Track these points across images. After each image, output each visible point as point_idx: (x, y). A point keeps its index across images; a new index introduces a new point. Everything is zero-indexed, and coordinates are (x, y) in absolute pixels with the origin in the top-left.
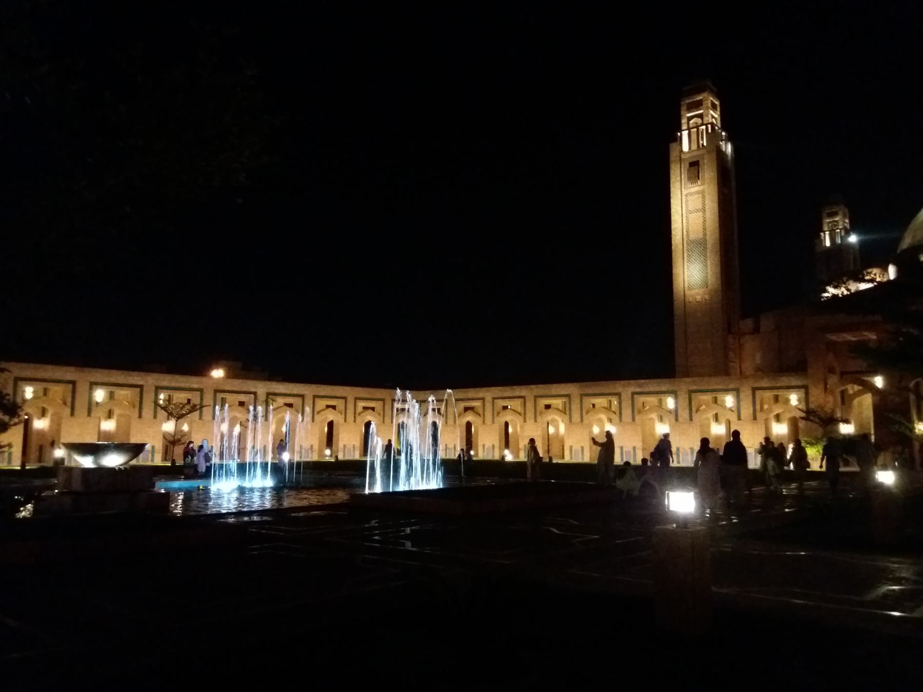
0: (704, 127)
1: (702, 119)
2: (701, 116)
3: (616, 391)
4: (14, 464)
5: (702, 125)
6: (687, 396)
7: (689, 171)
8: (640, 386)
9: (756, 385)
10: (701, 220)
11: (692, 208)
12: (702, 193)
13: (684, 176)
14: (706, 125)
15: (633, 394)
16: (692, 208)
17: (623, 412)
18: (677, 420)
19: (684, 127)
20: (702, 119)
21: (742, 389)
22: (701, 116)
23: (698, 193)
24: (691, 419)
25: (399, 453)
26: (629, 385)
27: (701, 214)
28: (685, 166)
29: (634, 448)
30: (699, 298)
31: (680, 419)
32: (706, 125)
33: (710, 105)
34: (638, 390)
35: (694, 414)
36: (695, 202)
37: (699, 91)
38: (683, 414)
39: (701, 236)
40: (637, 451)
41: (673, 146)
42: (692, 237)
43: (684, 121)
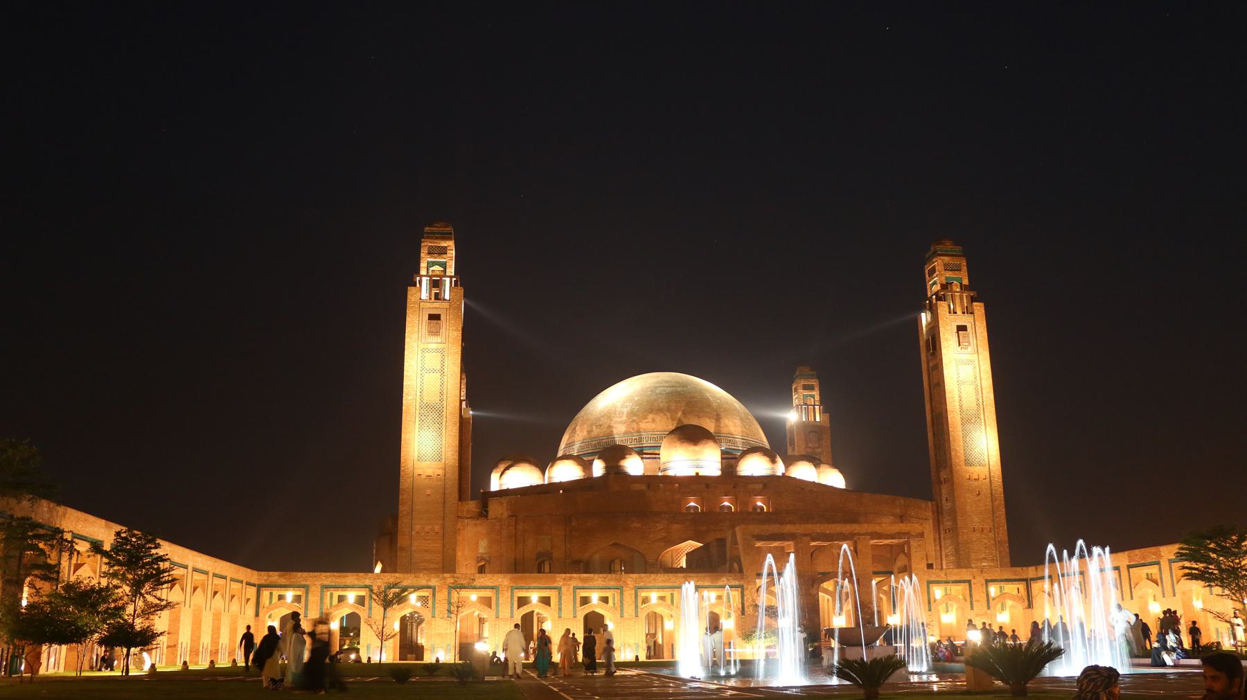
5: (445, 276)
11: (431, 367)
12: (442, 352)
16: (431, 367)
19: (423, 272)
26: (571, 578)
30: (429, 472)
34: (580, 585)
36: (433, 361)
37: (445, 237)
41: (411, 290)
42: (426, 399)
43: (423, 265)
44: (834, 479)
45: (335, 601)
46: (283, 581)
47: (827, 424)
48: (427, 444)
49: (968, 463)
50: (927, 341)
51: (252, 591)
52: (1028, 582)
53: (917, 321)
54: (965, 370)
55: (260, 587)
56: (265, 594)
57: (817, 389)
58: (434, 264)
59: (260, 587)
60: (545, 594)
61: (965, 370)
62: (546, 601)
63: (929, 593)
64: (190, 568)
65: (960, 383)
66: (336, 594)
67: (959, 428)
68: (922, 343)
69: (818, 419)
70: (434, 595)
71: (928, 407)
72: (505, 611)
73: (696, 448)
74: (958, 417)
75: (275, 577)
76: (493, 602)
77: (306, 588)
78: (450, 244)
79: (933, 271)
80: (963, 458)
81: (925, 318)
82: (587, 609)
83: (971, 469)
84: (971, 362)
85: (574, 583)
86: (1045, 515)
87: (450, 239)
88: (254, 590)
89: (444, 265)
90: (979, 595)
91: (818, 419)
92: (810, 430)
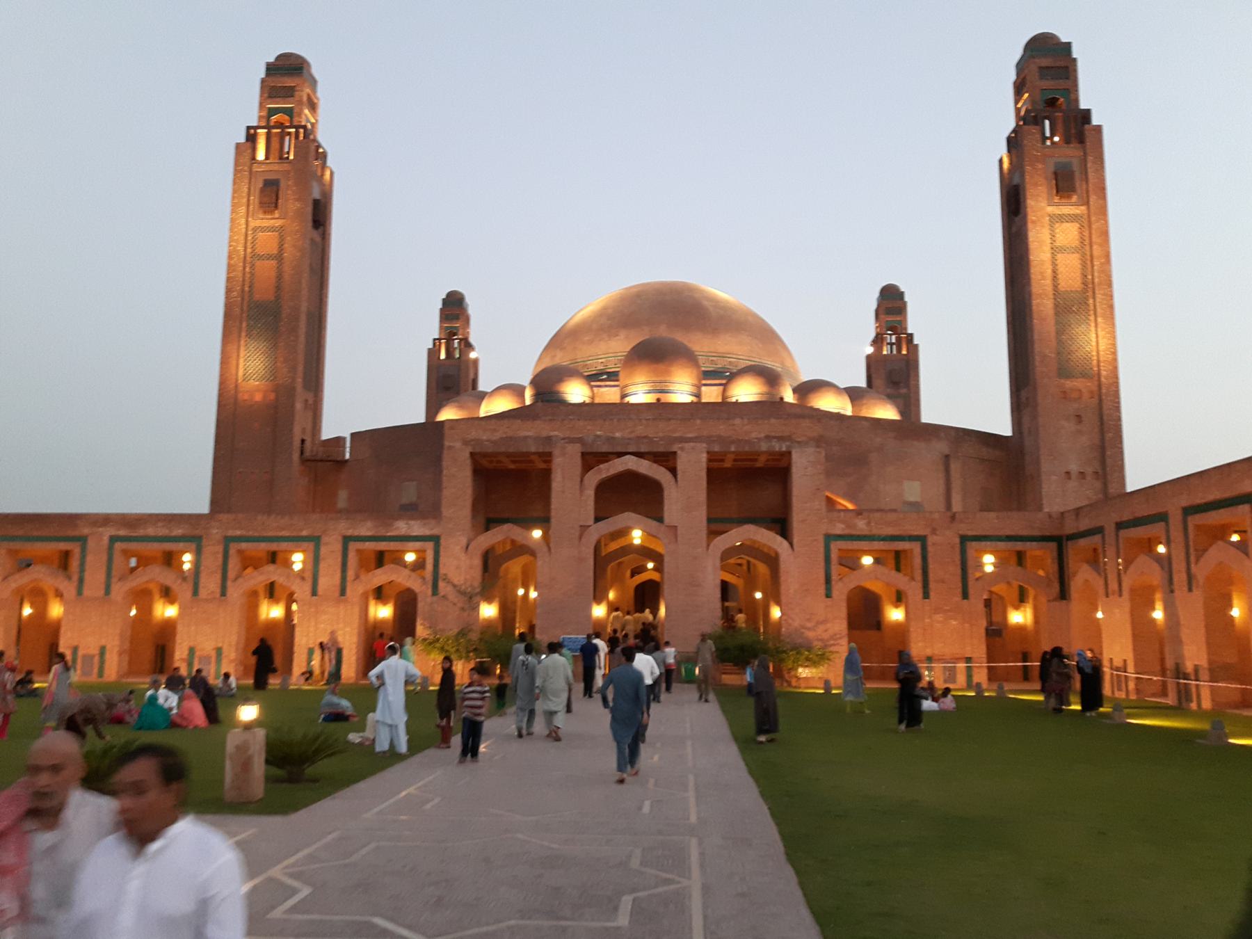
0: (293, 130)
1: (291, 117)
3: (76, 533)
4: (964, 671)
6: (220, 548)
7: (262, 191)
9: (350, 532)
10: (273, 274)
13: (254, 199)
14: (297, 127)
15: (114, 539)
17: (87, 575)
18: (195, 592)
20: (291, 117)
21: (325, 539)
22: (290, 112)
23: (272, 229)
24: (223, 593)
25: (480, 685)
27: (274, 263)
28: (260, 185)
29: (102, 650)
31: (203, 593)
32: (297, 127)
33: (305, 98)
34: (122, 533)
35: (229, 583)
38: (210, 584)
39: (270, 296)
40: (107, 656)
42: (257, 297)
65: (1055, 250)
73: (661, 366)
84: (1073, 218)
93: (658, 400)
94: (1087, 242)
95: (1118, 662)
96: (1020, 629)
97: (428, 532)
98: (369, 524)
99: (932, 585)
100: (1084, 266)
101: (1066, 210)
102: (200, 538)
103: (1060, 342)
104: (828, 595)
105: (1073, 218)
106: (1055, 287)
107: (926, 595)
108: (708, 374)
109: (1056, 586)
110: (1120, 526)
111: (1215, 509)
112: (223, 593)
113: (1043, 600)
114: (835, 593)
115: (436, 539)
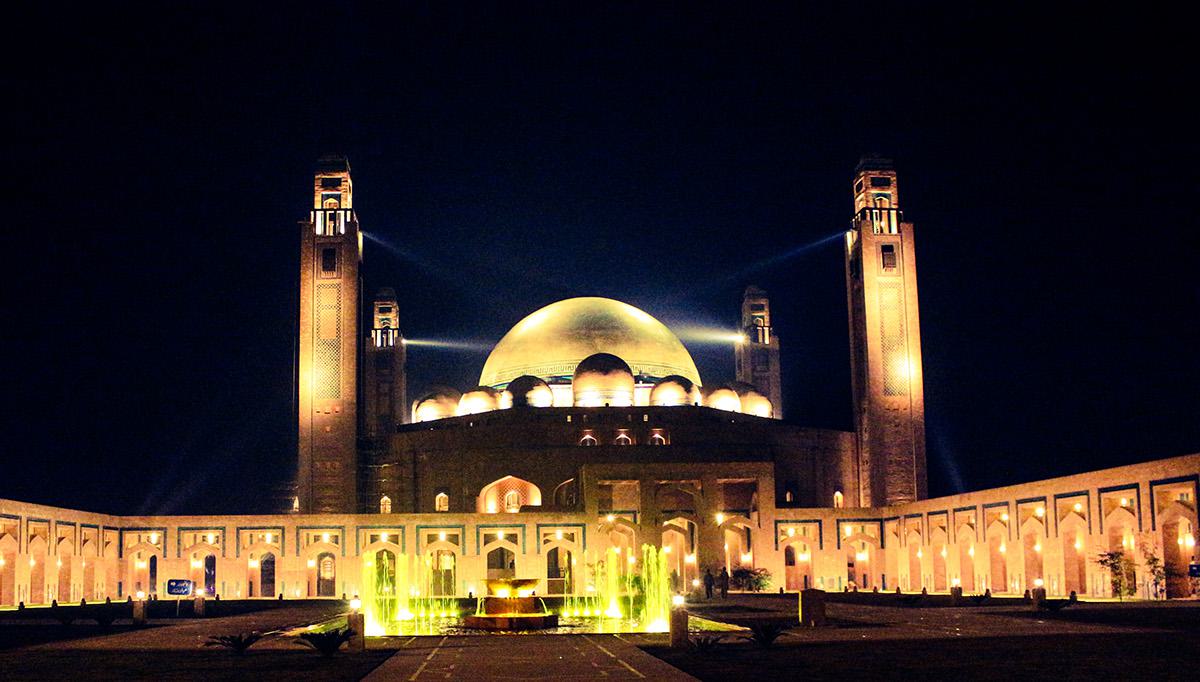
2: (338, 198)
5: (340, 209)
8: (424, 519)
15: (419, 527)
19: (318, 206)
26: (415, 518)
34: (423, 524)
43: (318, 199)
44: (760, 407)
45: (369, 540)
46: (142, 524)
47: (777, 347)
48: (321, 384)
49: (887, 392)
50: (851, 262)
51: (113, 536)
52: (881, 522)
53: (843, 241)
54: (890, 299)
55: (122, 531)
56: (890, 527)
57: (766, 309)
58: (328, 197)
59: (122, 531)
60: (511, 531)
61: (890, 299)
62: (395, 539)
63: (838, 528)
64: (24, 520)
66: (369, 533)
67: (880, 355)
68: (847, 265)
69: (767, 342)
70: (464, 533)
71: (851, 333)
72: (471, 545)
73: (608, 378)
74: (878, 344)
75: (136, 521)
76: (400, 538)
77: (402, 528)
78: (346, 177)
79: (860, 186)
80: (882, 387)
81: (850, 237)
82: (492, 547)
83: (890, 399)
84: (892, 285)
85: (418, 522)
86: (976, 443)
87: (344, 170)
88: (116, 534)
89: (338, 198)
90: (829, 535)
91: (767, 342)
92: (757, 355)
93: (607, 404)
94: (903, 302)
95: (904, 576)
96: (863, 563)
97: (579, 522)
98: (550, 517)
99: (824, 543)
100: (901, 320)
101: (891, 279)
102: (166, 528)
103: (885, 370)
104: (777, 549)
105: (892, 285)
106: (883, 337)
107: (821, 548)
108: (637, 379)
109: (880, 543)
110: (1019, 502)
111: (156, 572)
112: (478, 553)
113: (873, 548)
114: (779, 548)
115: (223, 529)
